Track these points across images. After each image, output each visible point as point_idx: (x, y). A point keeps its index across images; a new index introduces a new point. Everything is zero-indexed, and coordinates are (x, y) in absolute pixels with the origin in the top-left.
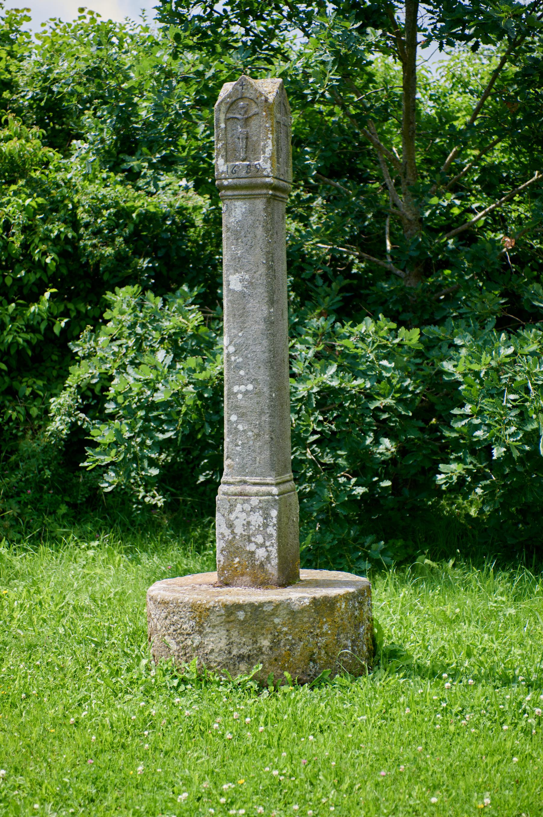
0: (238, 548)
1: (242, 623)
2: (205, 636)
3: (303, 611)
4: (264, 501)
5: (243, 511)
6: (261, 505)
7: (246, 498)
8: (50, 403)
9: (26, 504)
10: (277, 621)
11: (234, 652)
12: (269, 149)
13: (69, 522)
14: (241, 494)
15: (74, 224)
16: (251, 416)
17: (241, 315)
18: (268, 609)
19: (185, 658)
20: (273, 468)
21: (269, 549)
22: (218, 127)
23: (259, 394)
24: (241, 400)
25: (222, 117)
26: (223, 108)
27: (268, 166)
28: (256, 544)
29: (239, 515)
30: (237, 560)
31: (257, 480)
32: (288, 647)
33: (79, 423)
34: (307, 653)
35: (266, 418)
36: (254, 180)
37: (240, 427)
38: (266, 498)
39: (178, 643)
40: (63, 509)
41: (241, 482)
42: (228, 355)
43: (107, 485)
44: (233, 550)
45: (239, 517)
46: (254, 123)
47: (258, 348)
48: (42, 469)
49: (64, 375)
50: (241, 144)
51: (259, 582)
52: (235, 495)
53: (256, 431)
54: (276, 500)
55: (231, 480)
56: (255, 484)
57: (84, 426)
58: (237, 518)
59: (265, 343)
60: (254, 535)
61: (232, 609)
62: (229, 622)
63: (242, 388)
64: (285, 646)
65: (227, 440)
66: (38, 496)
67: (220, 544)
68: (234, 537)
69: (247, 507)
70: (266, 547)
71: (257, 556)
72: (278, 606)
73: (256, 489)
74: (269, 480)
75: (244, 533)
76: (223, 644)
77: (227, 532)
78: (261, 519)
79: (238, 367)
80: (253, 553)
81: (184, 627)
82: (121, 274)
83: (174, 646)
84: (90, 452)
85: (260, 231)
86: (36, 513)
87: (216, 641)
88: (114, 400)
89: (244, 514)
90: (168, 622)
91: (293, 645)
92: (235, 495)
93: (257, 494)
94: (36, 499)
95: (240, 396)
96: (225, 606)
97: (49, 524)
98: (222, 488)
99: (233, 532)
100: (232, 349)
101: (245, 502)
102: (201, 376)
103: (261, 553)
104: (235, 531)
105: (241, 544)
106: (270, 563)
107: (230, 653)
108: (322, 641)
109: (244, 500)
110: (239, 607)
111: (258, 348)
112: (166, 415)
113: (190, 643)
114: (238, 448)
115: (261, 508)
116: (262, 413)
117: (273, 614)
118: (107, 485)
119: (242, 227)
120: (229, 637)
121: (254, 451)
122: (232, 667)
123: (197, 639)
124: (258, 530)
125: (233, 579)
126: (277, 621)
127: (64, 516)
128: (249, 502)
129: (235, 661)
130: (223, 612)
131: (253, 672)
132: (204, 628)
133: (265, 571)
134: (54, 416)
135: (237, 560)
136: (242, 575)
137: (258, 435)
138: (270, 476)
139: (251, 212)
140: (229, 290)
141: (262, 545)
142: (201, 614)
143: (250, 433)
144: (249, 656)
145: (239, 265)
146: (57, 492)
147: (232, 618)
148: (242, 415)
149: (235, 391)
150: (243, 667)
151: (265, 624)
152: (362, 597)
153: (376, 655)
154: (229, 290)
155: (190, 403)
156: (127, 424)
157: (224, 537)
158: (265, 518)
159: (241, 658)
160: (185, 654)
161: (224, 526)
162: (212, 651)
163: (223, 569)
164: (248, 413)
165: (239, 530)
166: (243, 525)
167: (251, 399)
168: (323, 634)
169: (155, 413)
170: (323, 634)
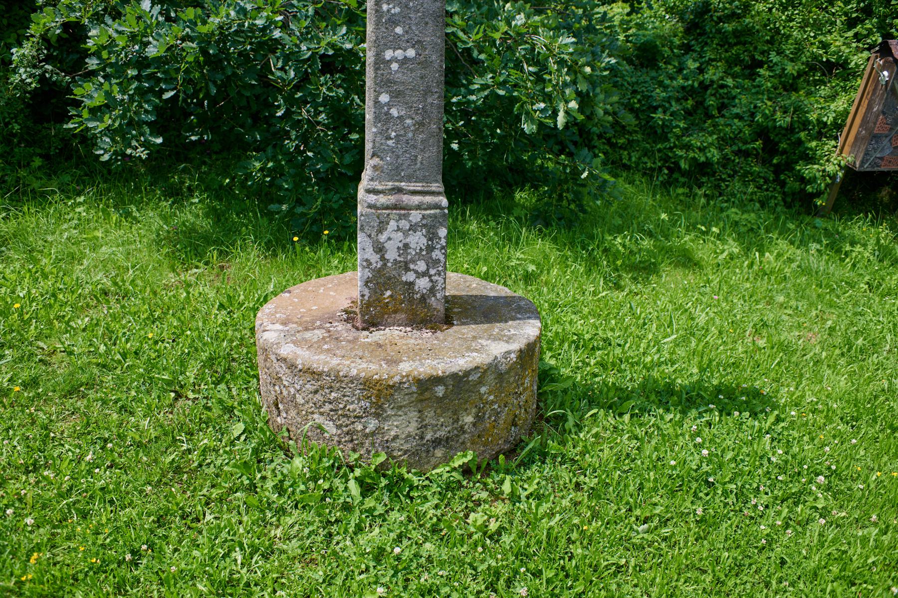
0: (389, 278)
1: (440, 400)
2: (385, 419)
4: (430, 216)
5: (399, 229)
6: (424, 222)
7: (403, 212)
8: (12, 54)
11: (428, 437)
13: (45, 174)
14: (395, 207)
16: (411, 96)
18: (473, 377)
19: (350, 445)
21: (434, 278)
23: (425, 64)
24: (396, 72)
28: (416, 272)
29: (393, 235)
30: (388, 293)
31: (418, 187)
32: (493, 418)
33: (47, 75)
37: (394, 112)
38: (432, 212)
39: (339, 427)
40: (37, 162)
41: (393, 189)
43: (102, 152)
48: (9, 123)
49: (26, 22)
51: (418, 319)
52: (387, 208)
53: (418, 118)
54: (444, 215)
55: (380, 188)
56: (414, 193)
57: (54, 79)
58: (389, 239)
60: (413, 261)
62: (422, 401)
64: (489, 418)
66: (8, 149)
68: (385, 265)
69: (405, 224)
70: (430, 276)
71: (416, 288)
72: (486, 371)
73: (417, 199)
75: (399, 259)
76: (412, 428)
77: (374, 258)
78: (424, 241)
79: (393, 21)
80: (412, 284)
81: (351, 407)
83: (330, 428)
84: (73, 112)
86: (8, 167)
87: (401, 426)
88: (97, 54)
89: (400, 234)
90: (318, 397)
91: (498, 413)
92: (387, 208)
93: (418, 207)
94: (5, 152)
95: (395, 66)
96: (419, 382)
97: (24, 177)
99: (382, 258)
101: (401, 217)
102: (203, 29)
104: (387, 257)
105: (394, 273)
106: (435, 296)
107: (422, 438)
109: (400, 215)
110: (437, 380)
112: (163, 73)
113: (359, 427)
114: (390, 142)
115: (424, 226)
116: (427, 92)
118: (102, 152)
120: (421, 419)
121: (415, 147)
122: (424, 455)
123: (373, 424)
124: (419, 254)
125: (383, 317)
126: (483, 390)
127: (39, 168)
130: (414, 389)
132: (384, 410)
133: (429, 307)
134: (16, 67)
135: (388, 293)
136: (395, 312)
137: (421, 124)
138: (437, 181)
141: (425, 274)
143: (409, 121)
144: (448, 438)
146: (29, 144)
147: (427, 395)
148: (396, 95)
149: (388, 57)
150: (439, 453)
151: (469, 397)
155: (190, 59)
156: (116, 84)
157: (371, 264)
158: (431, 239)
159: (437, 442)
160: (352, 441)
161: (370, 250)
162: (396, 437)
164: (407, 92)
166: (399, 248)
167: (412, 70)
169: (149, 71)
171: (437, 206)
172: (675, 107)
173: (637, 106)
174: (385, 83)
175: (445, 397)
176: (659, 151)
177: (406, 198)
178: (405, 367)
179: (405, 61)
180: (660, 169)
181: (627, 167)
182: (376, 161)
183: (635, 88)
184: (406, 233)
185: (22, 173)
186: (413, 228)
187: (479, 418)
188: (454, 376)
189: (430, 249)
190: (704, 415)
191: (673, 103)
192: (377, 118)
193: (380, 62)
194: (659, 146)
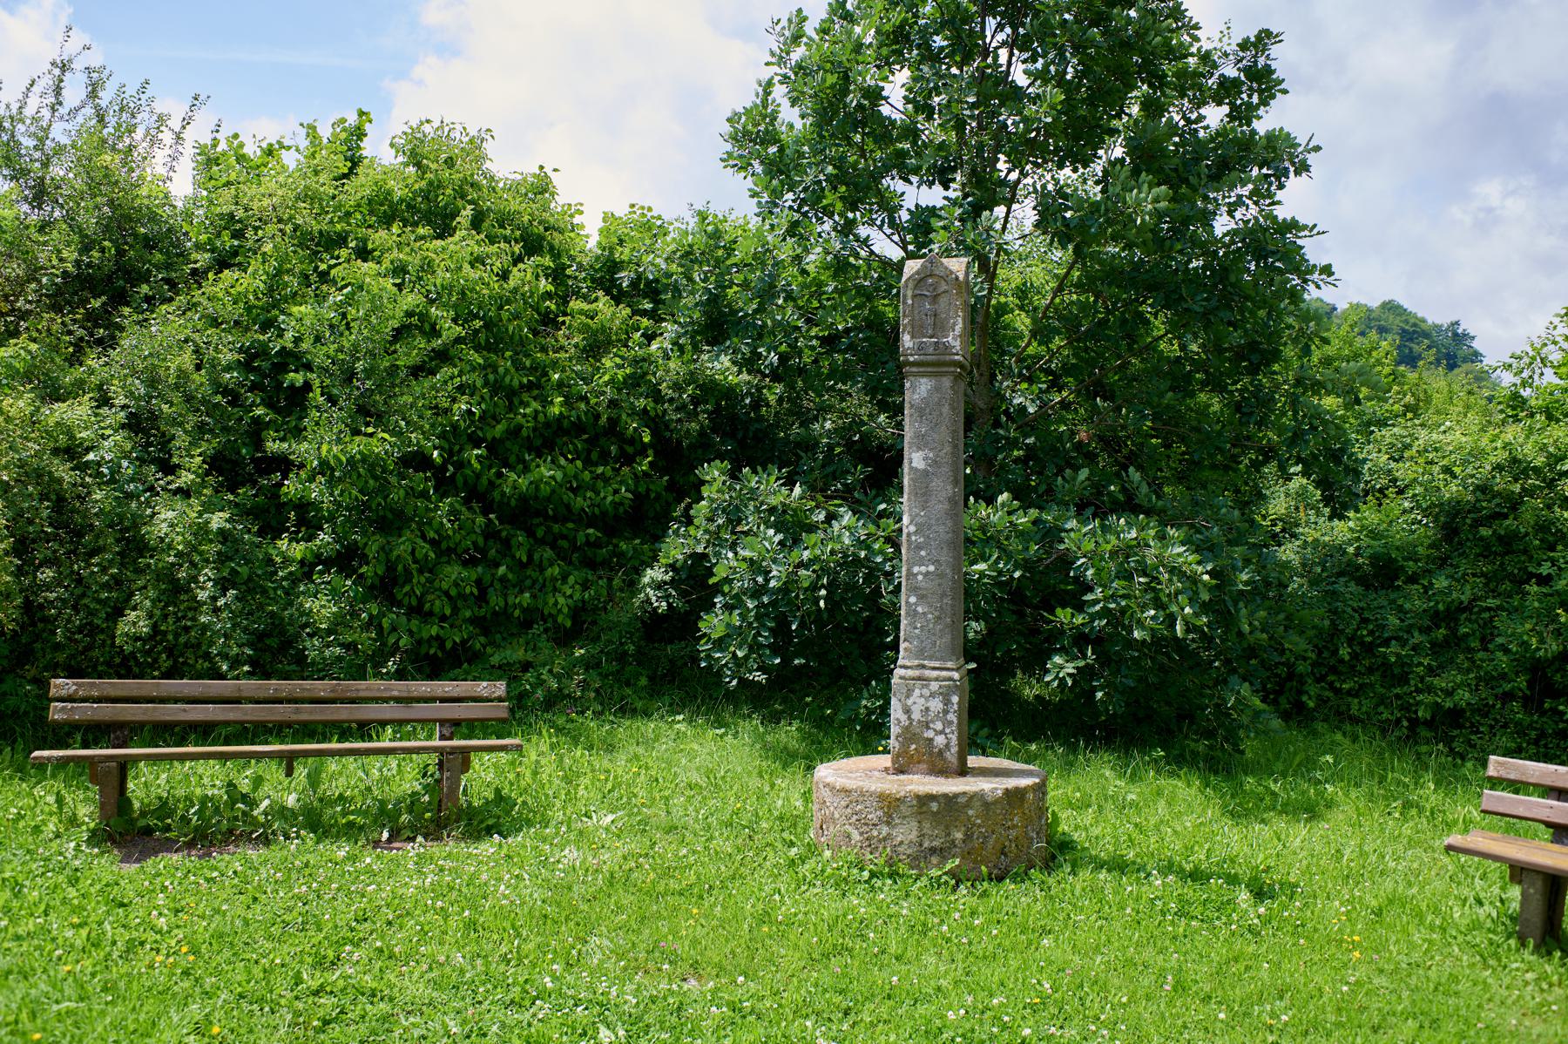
2: (894, 827)
3: (997, 802)
9: (607, 676)
10: (971, 812)
12: (959, 328)
14: (919, 679)
15: (657, 396)
17: (924, 494)
18: (962, 800)
20: (953, 653)
22: (905, 303)
23: (941, 576)
25: (909, 293)
26: (911, 285)
27: (957, 344)
31: (937, 664)
34: (999, 847)
35: (947, 600)
36: (942, 358)
37: (920, 609)
39: (861, 834)
40: (643, 681)
42: (909, 535)
44: (909, 735)
45: (917, 702)
46: (943, 300)
47: (941, 529)
50: (930, 321)
56: (934, 669)
59: (949, 523)
61: (924, 800)
63: (923, 569)
65: (904, 623)
67: (895, 730)
69: (926, 692)
72: (972, 797)
73: (935, 673)
74: (949, 665)
76: (913, 836)
77: (903, 718)
79: (919, 547)
82: (704, 450)
83: (856, 836)
85: (946, 410)
87: (905, 833)
93: (937, 679)
95: (920, 577)
96: (918, 797)
98: (898, 672)
100: (912, 529)
101: (923, 687)
103: (940, 740)
108: (1013, 833)
110: (931, 797)
111: (941, 529)
113: (875, 833)
117: (968, 805)
119: (927, 404)
120: (920, 829)
123: (885, 830)
126: (971, 812)
128: (924, 687)
129: (923, 856)
131: (948, 867)
133: (945, 760)
137: (939, 618)
139: (937, 389)
140: (911, 468)
141: (942, 732)
142: (891, 806)
145: (921, 442)
148: (921, 597)
150: (935, 860)
152: (1041, 789)
153: (1058, 852)
154: (911, 468)
159: (933, 851)
163: (898, 755)
165: (916, 716)
168: (1015, 826)
170: (1015, 826)
171: (950, 679)
172: (1417, 638)
173: (1369, 639)
174: (914, 590)
175: (938, 812)
176: (1398, 696)
177: (928, 673)
178: (909, 788)
179: (927, 574)
180: (1398, 721)
181: (1355, 720)
182: (906, 644)
183: (1366, 615)
184: (927, 699)
185: (629, 691)
186: (932, 695)
187: (968, 837)
188: (945, 796)
189: (946, 712)
190: (525, 397)
191: (1416, 634)
192: (908, 614)
193: (910, 575)
194: (1398, 690)
